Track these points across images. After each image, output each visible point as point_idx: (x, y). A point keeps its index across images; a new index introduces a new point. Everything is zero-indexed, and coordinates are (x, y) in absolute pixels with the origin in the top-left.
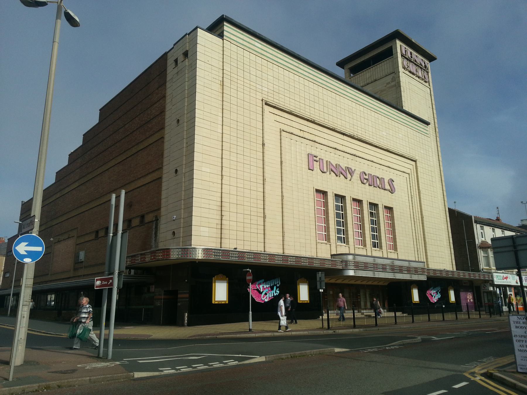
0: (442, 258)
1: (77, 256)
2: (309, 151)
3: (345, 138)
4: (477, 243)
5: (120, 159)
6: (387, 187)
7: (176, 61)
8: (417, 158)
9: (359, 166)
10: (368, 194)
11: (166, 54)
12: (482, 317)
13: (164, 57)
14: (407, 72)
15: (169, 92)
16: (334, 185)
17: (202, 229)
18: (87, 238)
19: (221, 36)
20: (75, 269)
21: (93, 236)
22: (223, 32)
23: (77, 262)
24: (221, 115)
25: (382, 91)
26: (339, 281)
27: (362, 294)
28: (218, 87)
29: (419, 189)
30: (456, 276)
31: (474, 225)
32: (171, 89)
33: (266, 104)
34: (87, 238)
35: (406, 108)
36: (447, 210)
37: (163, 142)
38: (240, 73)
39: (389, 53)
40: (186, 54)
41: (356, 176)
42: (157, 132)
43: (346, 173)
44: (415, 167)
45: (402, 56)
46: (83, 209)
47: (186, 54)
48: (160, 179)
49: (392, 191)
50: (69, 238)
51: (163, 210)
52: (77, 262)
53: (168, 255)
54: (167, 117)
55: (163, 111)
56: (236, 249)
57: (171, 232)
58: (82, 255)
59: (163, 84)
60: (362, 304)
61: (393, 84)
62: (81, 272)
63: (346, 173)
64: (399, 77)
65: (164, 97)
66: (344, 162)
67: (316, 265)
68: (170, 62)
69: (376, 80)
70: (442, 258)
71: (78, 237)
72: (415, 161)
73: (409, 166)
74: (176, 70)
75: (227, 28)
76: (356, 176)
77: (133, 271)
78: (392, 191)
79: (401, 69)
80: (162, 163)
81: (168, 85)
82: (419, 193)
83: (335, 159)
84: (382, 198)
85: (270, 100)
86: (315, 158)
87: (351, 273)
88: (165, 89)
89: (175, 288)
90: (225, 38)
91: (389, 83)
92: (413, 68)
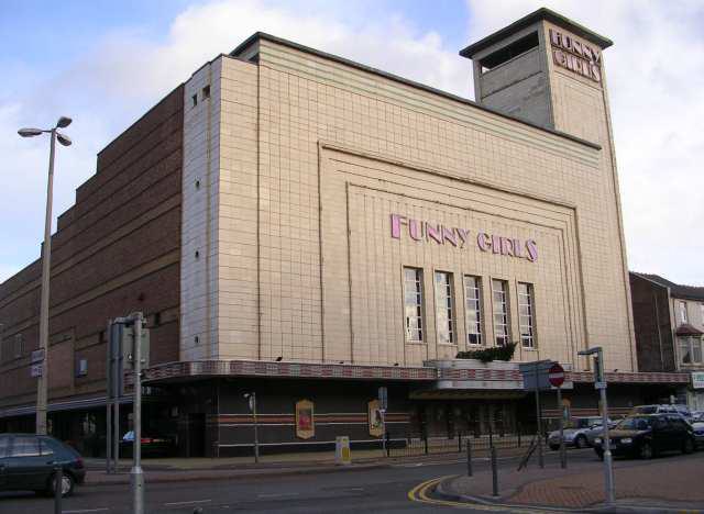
0: (620, 359)
1: (76, 365)
2: (394, 210)
3: (455, 184)
4: (673, 327)
5: (126, 230)
6: (524, 253)
7: (195, 97)
8: (576, 204)
9: (473, 226)
10: (493, 267)
11: (183, 85)
12: (430, 451)
13: (181, 89)
14: (563, 71)
15: (187, 140)
16: (431, 257)
17: (233, 333)
18: (90, 342)
19: (255, 60)
20: (77, 385)
21: (96, 339)
22: (258, 55)
23: (78, 376)
24: (255, 172)
25: (525, 99)
26: (436, 396)
27: (481, 414)
28: (252, 134)
29: (579, 252)
30: (636, 380)
31: (670, 300)
32: (192, 138)
33: (324, 148)
34: (90, 342)
35: (559, 128)
36: (627, 277)
37: (180, 212)
38: (284, 108)
39: (532, 42)
40: (207, 90)
41: (471, 241)
42: (172, 196)
43: (456, 238)
44: (573, 218)
45: (553, 45)
46: (82, 299)
47: (207, 90)
48: (178, 263)
49: (531, 259)
50: (65, 340)
51: (183, 306)
52: (78, 376)
53: (188, 369)
54: (185, 175)
55: (179, 168)
56: (280, 359)
57: (193, 338)
58: (83, 364)
59: (179, 129)
60: (482, 426)
61: (540, 89)
62: (83, 390)
63: (456, 238)
64: (548, 79)
65: (181, 148)
66: (450, 220)
67: (379, 375)
68: (188, 98)
69: (516, 82)
70: (620, 359)
71: (77, 340)
72: (574, 209)
73: (562, 218)
74: (195, 111)
75: (264, 48)
76: (471, 241)
77: (149, 389)
78: (531, 259)
79: (551, 66)
80: (180, 240)
81: (186, 131)
82: (580, 257)
83: (434, 218)
84: (513, 270)
85: (331, 143)
86: (402, 220)
87: (448, 385)
88: (182, 136)
89: (196, 410)
90: (261, 62)
91: (535, 88)
92: (573, 63)
